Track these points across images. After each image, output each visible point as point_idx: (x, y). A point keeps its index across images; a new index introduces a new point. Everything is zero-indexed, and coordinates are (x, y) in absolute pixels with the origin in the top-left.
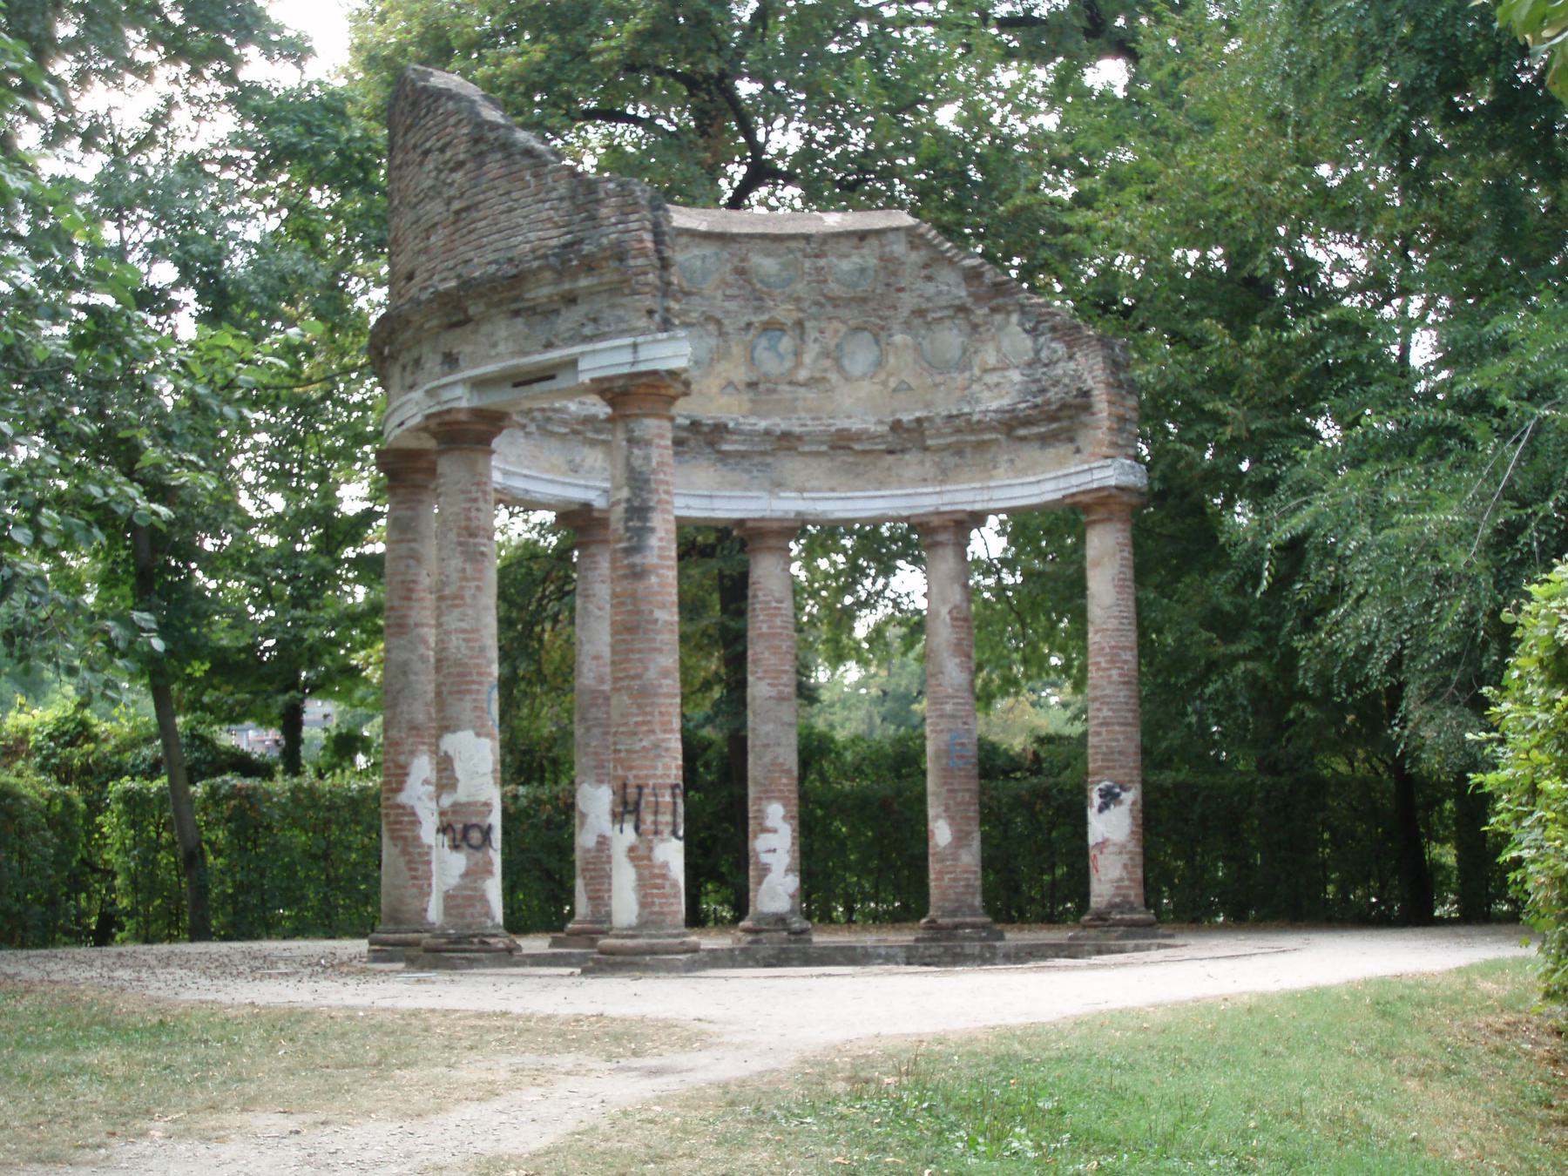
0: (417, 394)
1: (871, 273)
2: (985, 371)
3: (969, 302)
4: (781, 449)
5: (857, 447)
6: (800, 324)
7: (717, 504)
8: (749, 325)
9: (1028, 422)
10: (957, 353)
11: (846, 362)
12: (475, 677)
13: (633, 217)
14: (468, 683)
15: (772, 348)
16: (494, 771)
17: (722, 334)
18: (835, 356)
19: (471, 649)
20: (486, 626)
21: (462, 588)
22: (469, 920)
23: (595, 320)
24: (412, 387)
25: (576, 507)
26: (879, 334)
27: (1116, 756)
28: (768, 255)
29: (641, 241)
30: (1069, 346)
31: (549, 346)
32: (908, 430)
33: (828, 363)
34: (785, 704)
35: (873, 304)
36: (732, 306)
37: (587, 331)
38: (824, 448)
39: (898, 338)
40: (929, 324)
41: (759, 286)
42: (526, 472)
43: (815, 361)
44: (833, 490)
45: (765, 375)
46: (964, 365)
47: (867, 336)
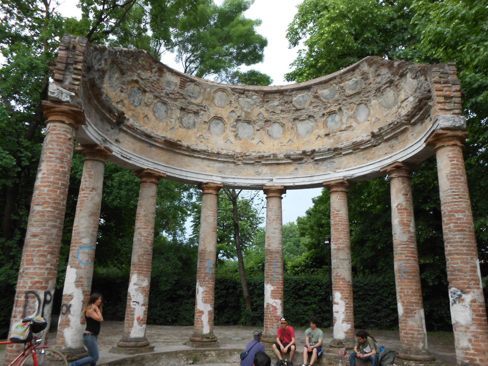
1: (360, 82)
2: (402, 102)
6: (340, 109)
7: (314, 178)
8: (324, 114)
11: (358, 118)
15: (333, 120)
16: (88, 278)
17: (316, 121)
27: (457, 273)
28: (325, 89)
33: (352, 120)
34: (341, 252)
35: (362, 93)
36: (316, 110)
38: (351, 151)
41: (324, 100)
43: (347, 120)
44: (355, 166)
47: (363, 105)
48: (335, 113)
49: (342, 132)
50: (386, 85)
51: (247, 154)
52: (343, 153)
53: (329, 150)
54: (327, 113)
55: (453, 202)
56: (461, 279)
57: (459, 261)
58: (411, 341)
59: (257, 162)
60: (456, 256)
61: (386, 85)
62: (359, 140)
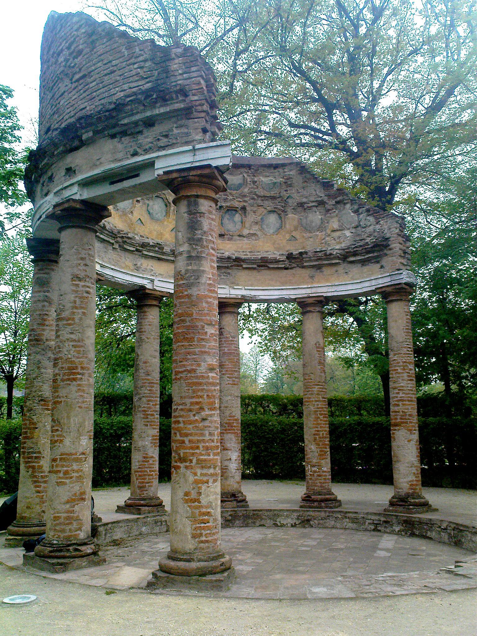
0: (50, 197)
2: (333, 231)
3: (325, 199)
4: (235, 266)
5: (271, 266)
9: (355, 254)
10: (319, 222)
12: (79, 370)
13: (194, 69)
14: (74, 374)
18: (260, 223)
19: (79, 352)
20: (88, 337)
21: (73, 313)
22: (68, 534)
23: (166, 136)
24: (46, 195)
25: (138, 288)
26: (281, 213)
29: (199, 83)
30: (376, 218)
31: (135, 154)
32: (295, 258)
37: (161, 144)
38: (255, 266)
39: (290, 215)
40: (305, 209)
42: (112, 267)
45: (228, 231)
46: (321, 228)
48: (236, 211)
49: (241, 238)
50: (314, 204)
51: (130, 235)
52: (244, 266)
53: (229, 258)
54: (227, 207)
55: (407, 354)
56: (411, 422)
57: (410, 407)
58: (324, 483)
59: (137, 250)
60: (407, 403)
61: (314, 204)
62: (270, 256)
